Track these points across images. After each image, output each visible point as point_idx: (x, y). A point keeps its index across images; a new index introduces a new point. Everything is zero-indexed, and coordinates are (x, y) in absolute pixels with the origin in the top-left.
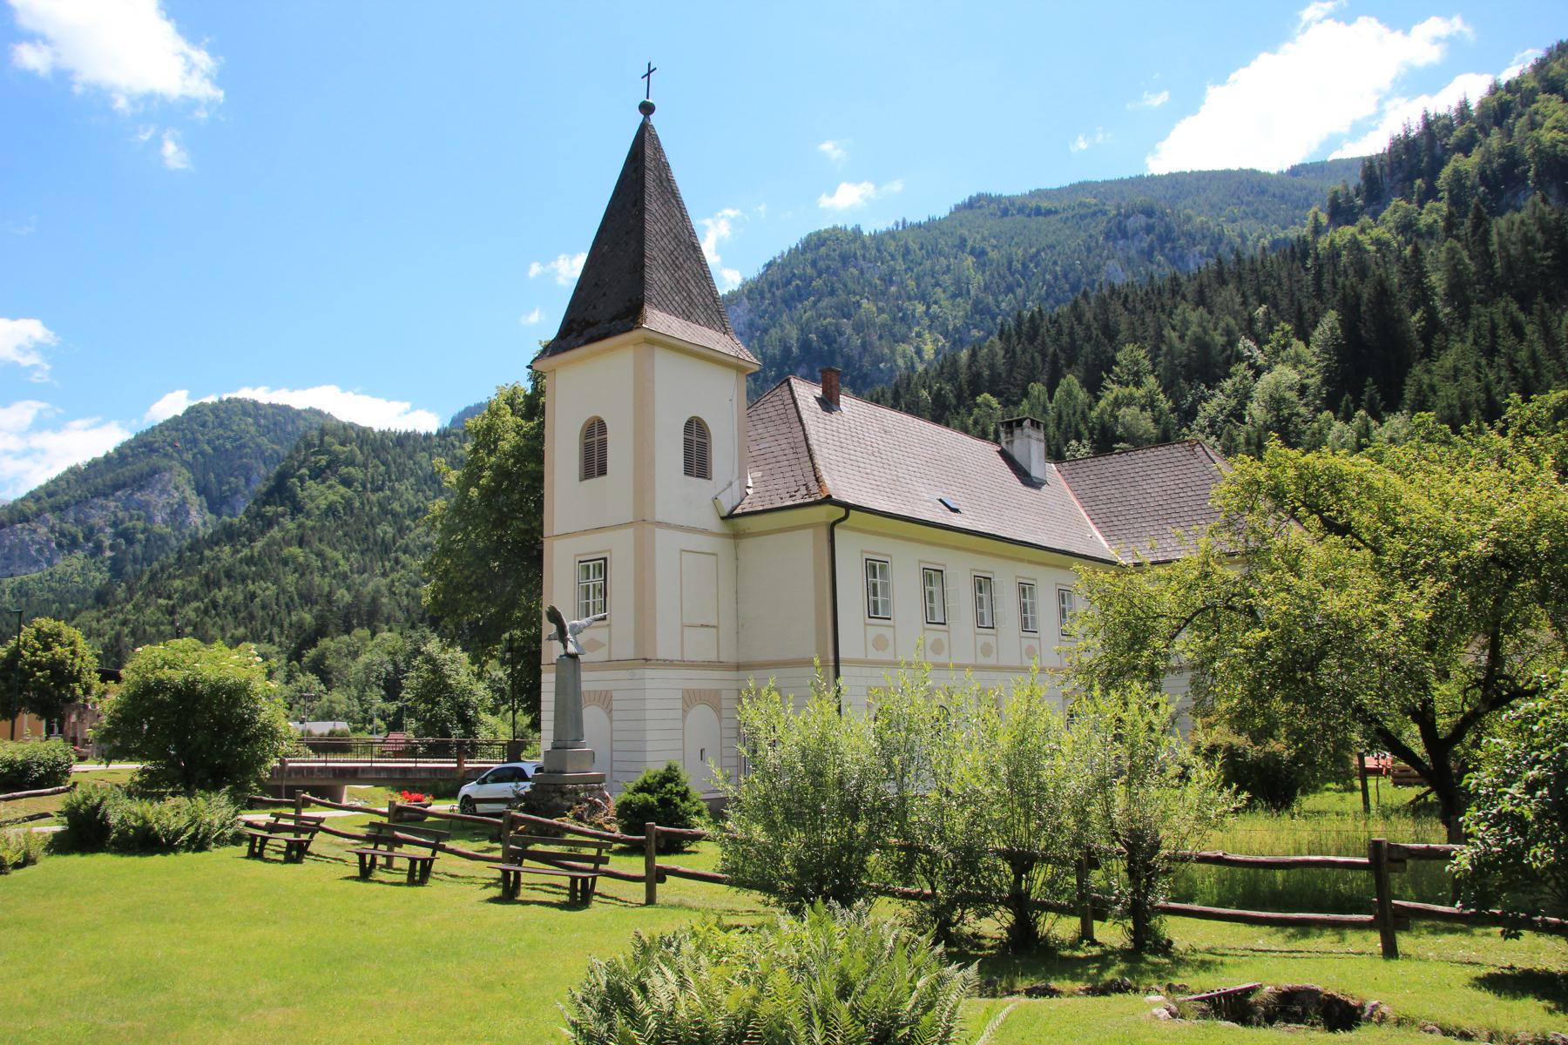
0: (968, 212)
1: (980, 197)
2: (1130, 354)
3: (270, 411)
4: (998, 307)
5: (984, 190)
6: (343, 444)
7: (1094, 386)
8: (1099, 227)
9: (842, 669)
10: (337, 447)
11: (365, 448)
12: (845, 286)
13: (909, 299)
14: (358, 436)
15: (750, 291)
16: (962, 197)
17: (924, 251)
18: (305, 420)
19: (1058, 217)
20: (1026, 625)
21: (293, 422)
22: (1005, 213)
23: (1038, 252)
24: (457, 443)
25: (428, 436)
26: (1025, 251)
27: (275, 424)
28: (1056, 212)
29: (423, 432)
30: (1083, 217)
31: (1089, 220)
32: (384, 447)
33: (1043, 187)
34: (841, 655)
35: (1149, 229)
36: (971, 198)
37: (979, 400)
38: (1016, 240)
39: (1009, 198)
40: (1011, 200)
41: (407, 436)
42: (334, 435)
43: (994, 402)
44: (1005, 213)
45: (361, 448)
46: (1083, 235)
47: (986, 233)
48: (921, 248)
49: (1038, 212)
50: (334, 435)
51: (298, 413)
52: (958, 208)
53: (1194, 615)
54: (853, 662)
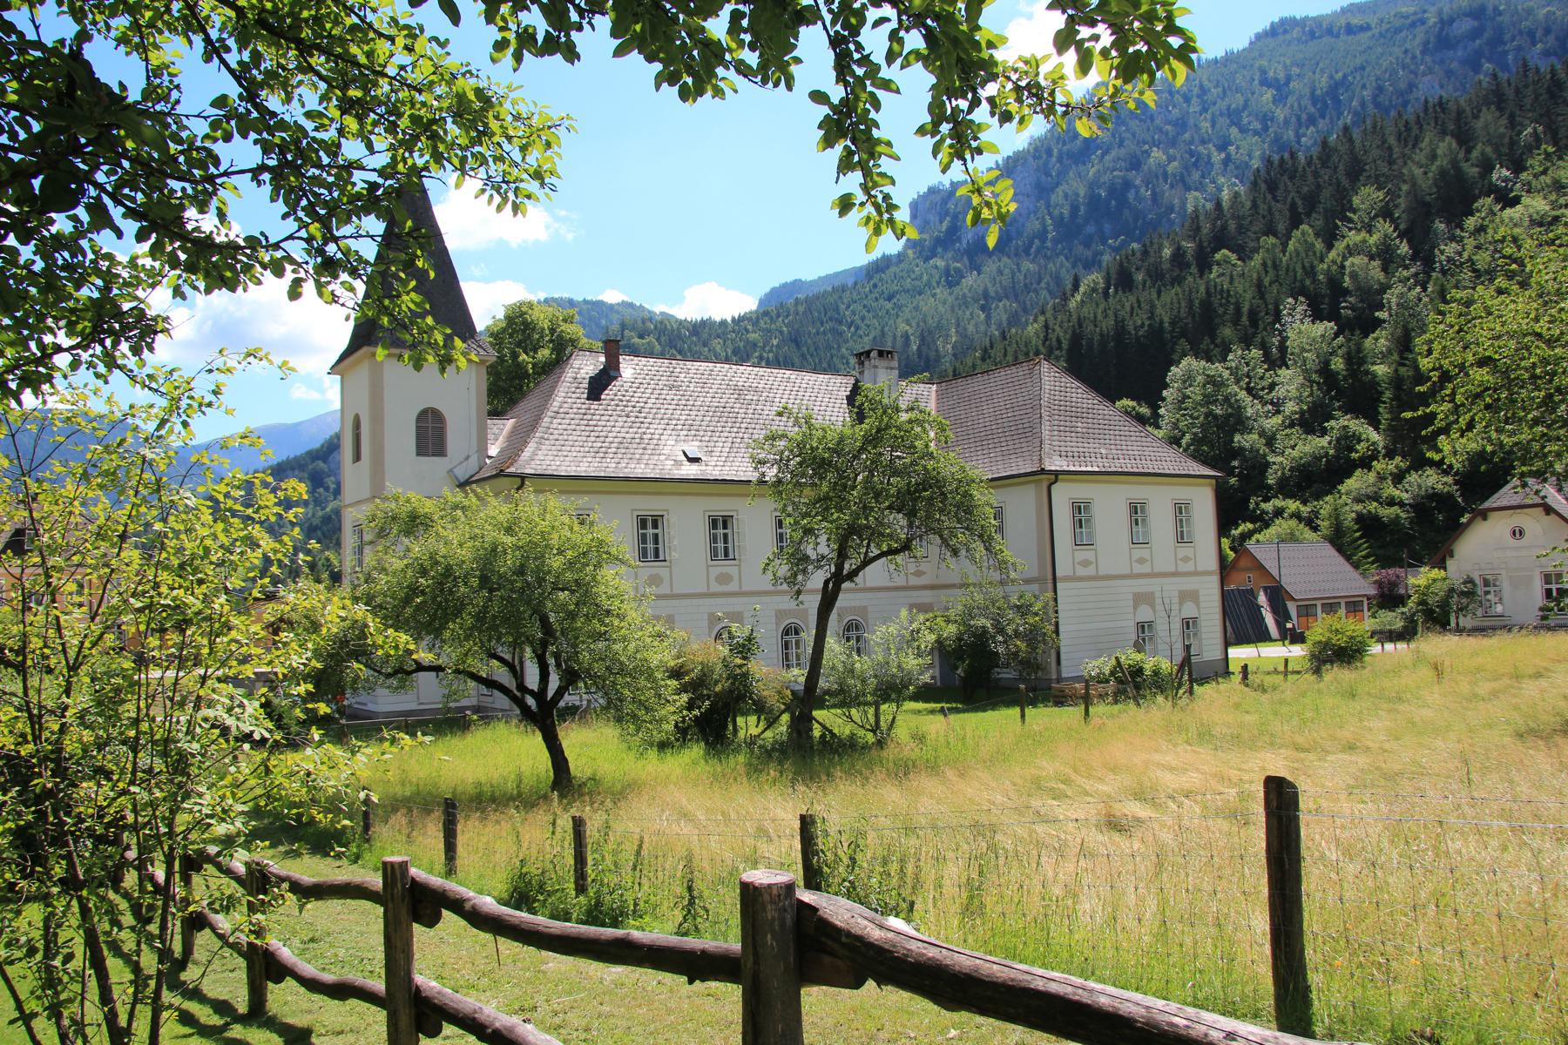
0: (1270, 40)
1: (1283, 22)
2: (1366, 197)
3: (585, 307)
4: (1298, 142)
5: (1287, 13)
6: (641, 337)
7: (1330, 238)
8: (1415, 41)
9: (1059, 585)
10: (636, 340)
11: (663, 339)
12: (1134, 135)
13: (1203, 142)
14: (656, 328)
15: (1036, 150)
16: (1262, 24)
17: (1220, 89)
18: (618, 312)
19: (1369, 34)
20: (1181, 538)
21: (607, 316)
22: (1312, 35)
23: (1345, 76)
24: (750, 327)
25: (723, 323)
26: (1331, 77)
27: (590, 319)
28: (1368, 28)
29: (718, 319)
30: (1398, 31)
31: (1404, 34)
32: (680, 337)
33: (1299, 12)
34: (1058, 574)
35: (1476, 33)
36: (1272, 24)
37: (1218, 256)
38: (1321, 65)
39: (1314, 19)
40: (1318, 20)
41: (704, 323)
42: (633, 329)
43: (1233, 257)
44: (1312, 35)
45: (658, 340)
46: (1398, 51)
47: (1288, 62)
48: (1216, 86)
49: (1350, 30)
50: (633, 329)
51: (611, 307)
52: (1258, 37)
53: (948, 545)
54: (1067, 579)
